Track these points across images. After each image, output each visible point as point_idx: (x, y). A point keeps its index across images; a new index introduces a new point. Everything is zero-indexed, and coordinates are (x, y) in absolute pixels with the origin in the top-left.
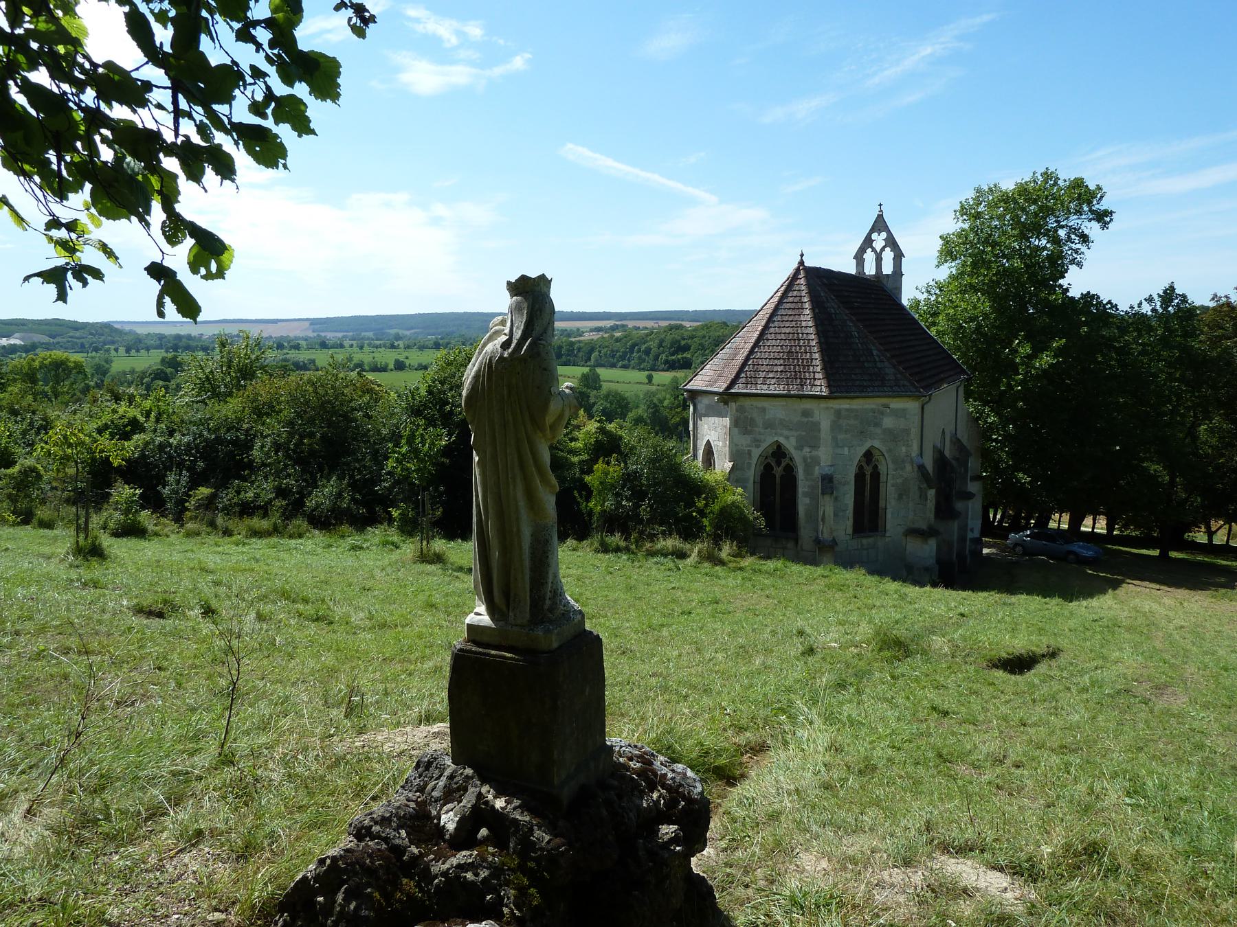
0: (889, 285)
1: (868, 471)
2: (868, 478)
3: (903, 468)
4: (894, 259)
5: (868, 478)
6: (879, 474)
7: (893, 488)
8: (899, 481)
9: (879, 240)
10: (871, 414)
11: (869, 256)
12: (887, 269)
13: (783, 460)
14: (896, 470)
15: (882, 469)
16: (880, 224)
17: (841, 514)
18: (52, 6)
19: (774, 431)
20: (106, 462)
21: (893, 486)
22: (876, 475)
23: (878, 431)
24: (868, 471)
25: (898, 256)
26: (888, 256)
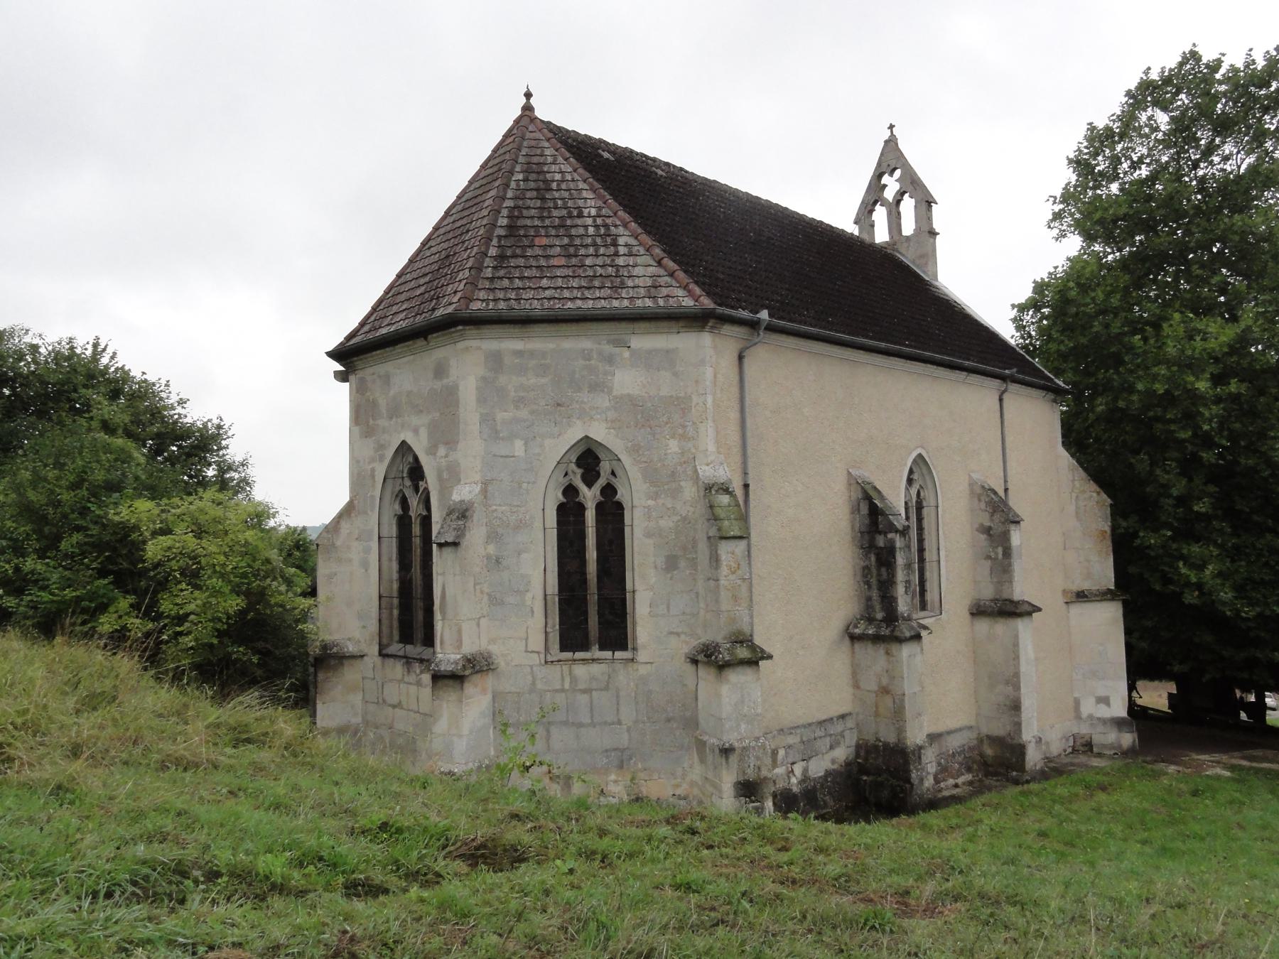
0: (907, 257)
1: (590, 496)
2: (590, 515)
3: (675, 493)
4: (916, 207)
5: (590, 515)
6: (620, 506)
7: (650, 541)
8: (667, 523)
9: (892, 185)
10: (582, 362)
11: (880, 215)
12: (908, 227)
13: (421, 483)
14: (655, 496)
15: (622, 495)
16: (891, 158)
17: (511, 599)
18: (1158, 588)
19: (399, 420)
20: (1020, 750)
21: (648, 535)
22: (612, 511)
23: (603, 401)
24: (590, 496)
25: (926, 202)
26: (908, 206)
